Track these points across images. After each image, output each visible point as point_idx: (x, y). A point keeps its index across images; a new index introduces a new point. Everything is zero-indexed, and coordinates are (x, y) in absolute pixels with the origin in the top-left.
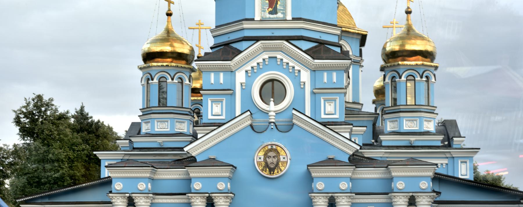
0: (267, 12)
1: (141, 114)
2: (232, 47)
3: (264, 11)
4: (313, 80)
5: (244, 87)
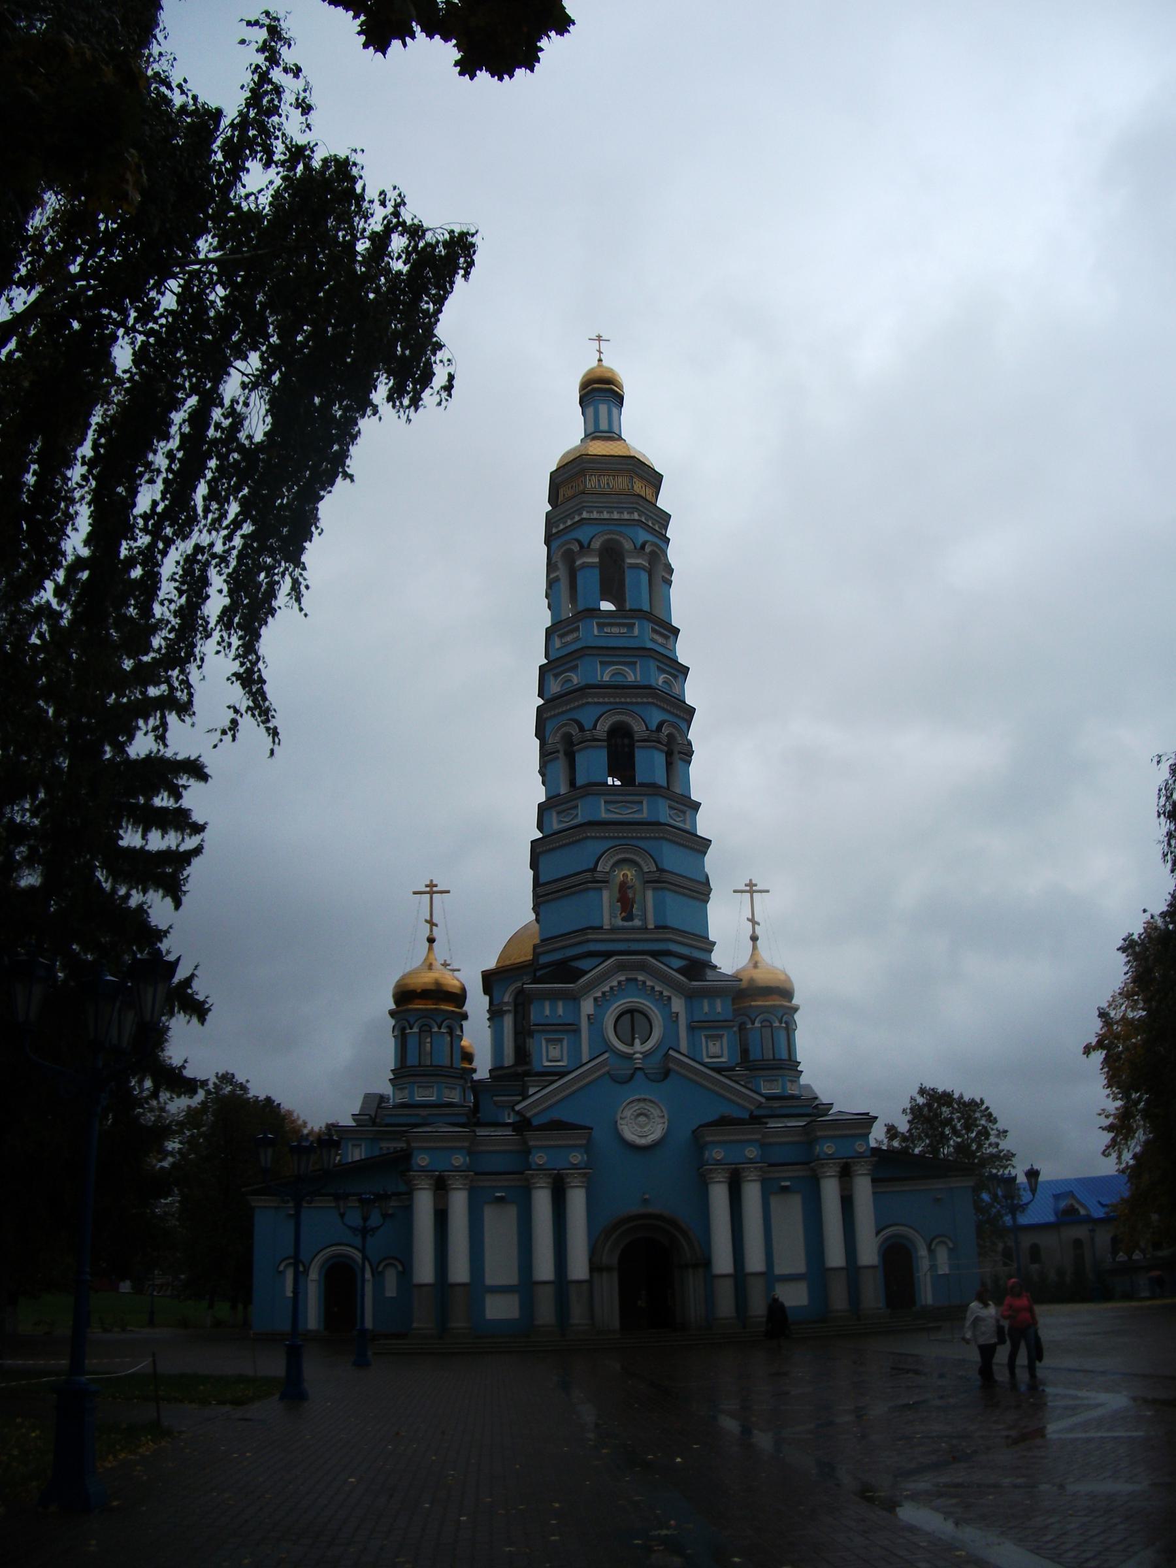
0: (620, 918)
1: (392, 1077)
2: (577, 968)
4: (690, 1010)
5: (592, 1021)
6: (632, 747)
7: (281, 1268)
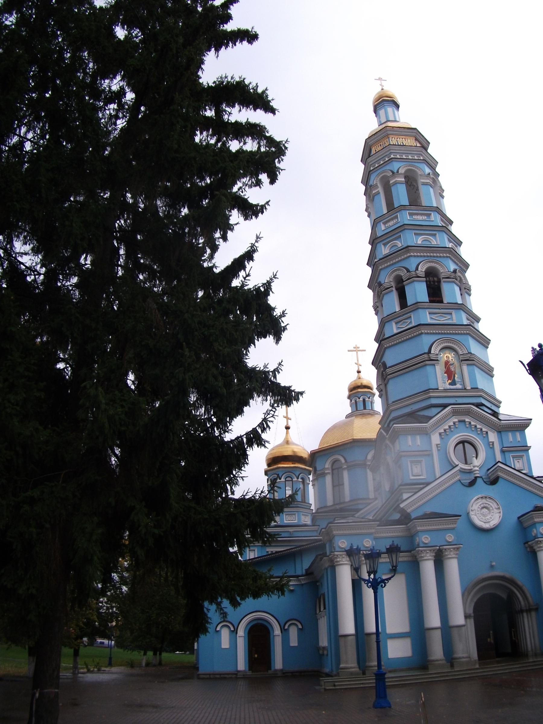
3: (445, 383)
5: (439, 449)
6: (439, 282)
7: (218, 629)
